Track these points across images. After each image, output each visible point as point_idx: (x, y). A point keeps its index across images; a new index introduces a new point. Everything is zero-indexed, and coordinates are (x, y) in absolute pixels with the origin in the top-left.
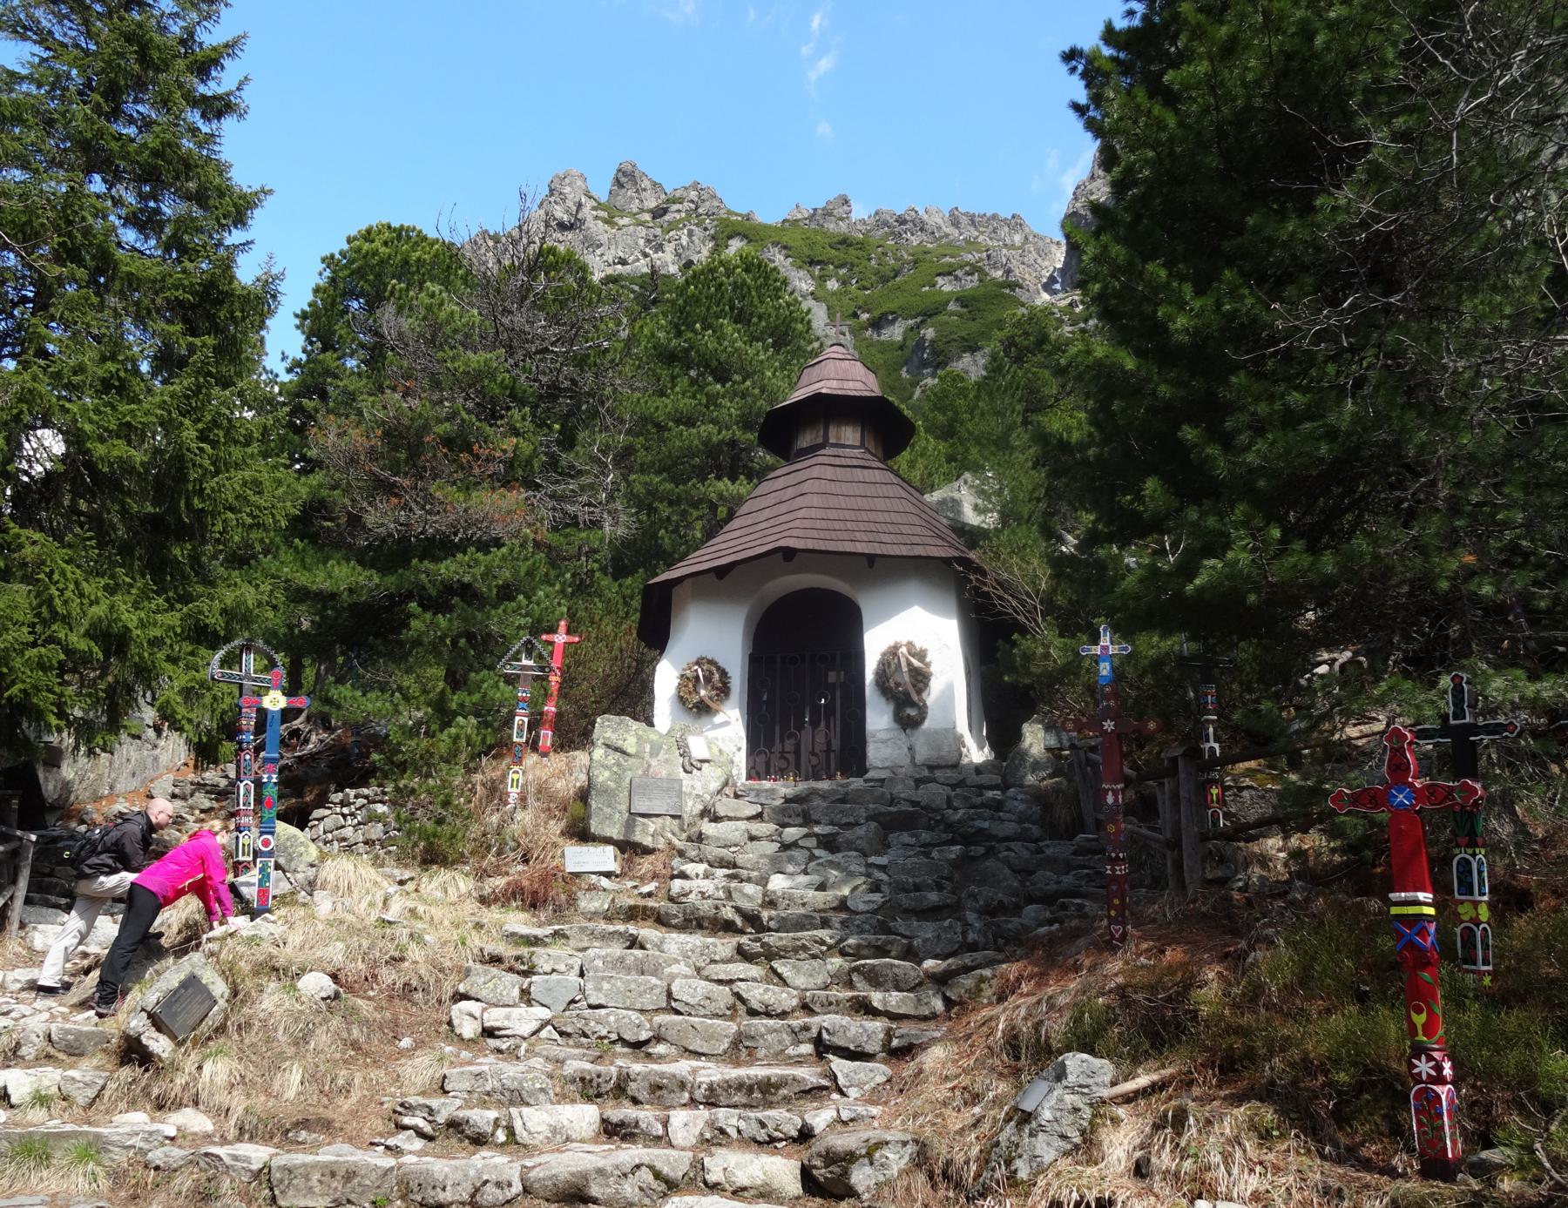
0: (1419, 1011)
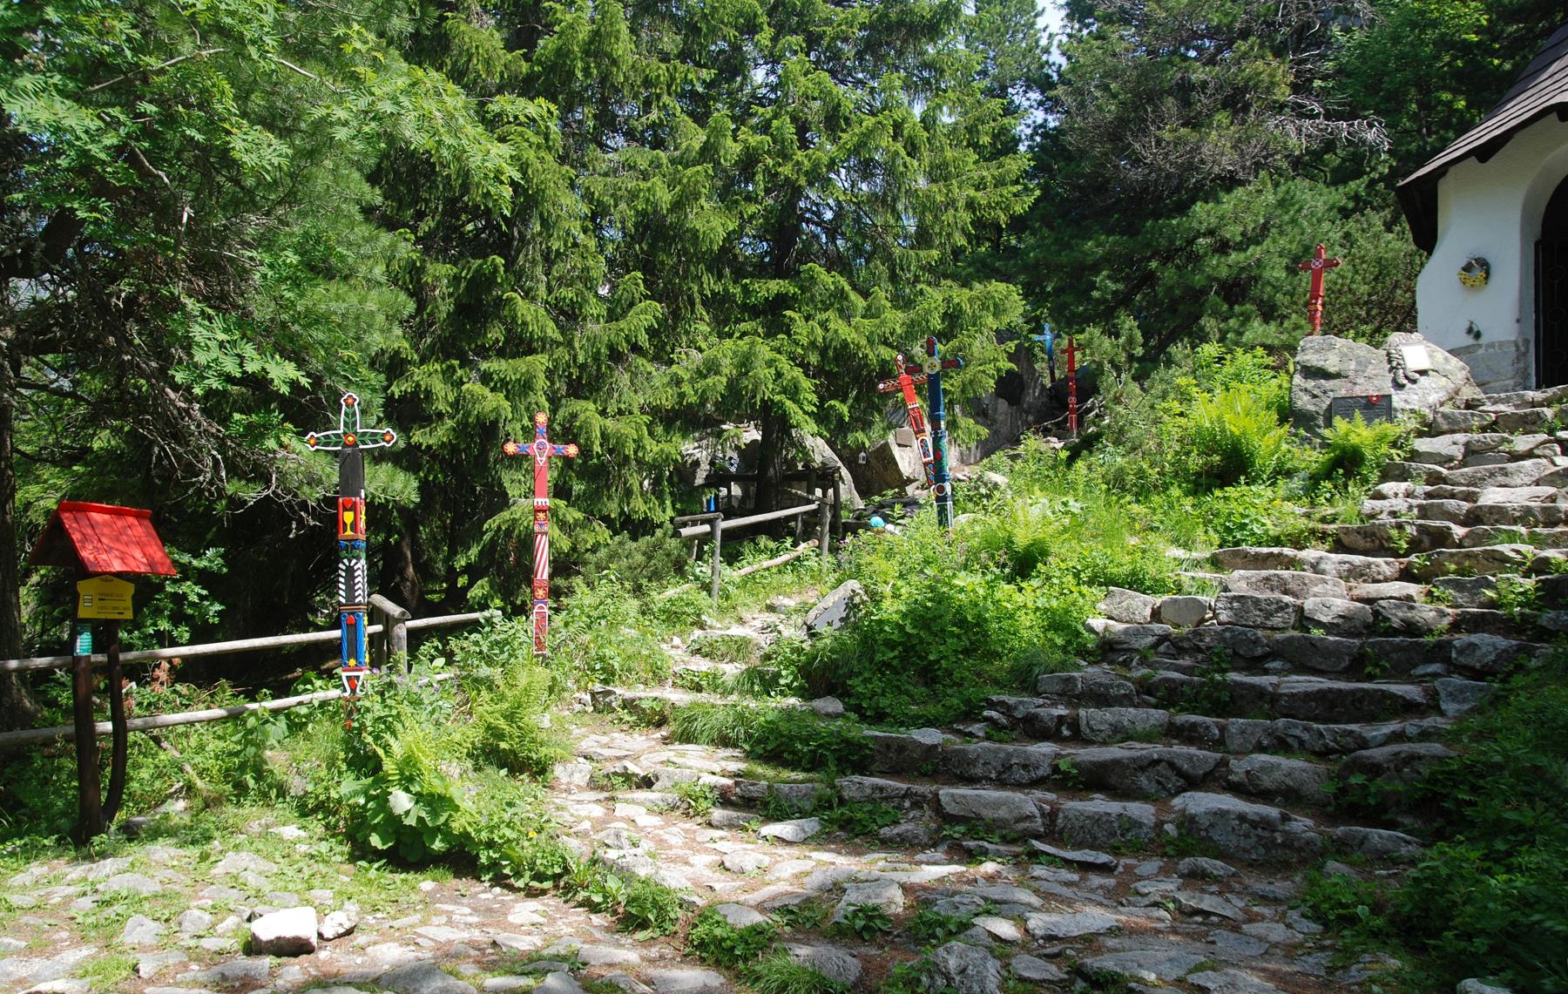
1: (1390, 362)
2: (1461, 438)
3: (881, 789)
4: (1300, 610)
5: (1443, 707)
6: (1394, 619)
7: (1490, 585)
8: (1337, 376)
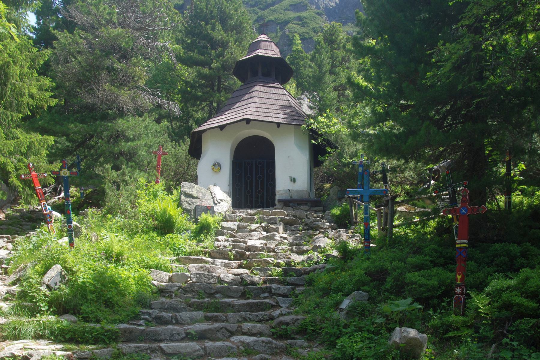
0: (459, 275)
1: (212, 195)
2: (237, 223)
3: (139, 347)
4: (219, 278)
5: (281, 305)
6: (248, 280)
7: (269, 270)
8: (196, 198)
